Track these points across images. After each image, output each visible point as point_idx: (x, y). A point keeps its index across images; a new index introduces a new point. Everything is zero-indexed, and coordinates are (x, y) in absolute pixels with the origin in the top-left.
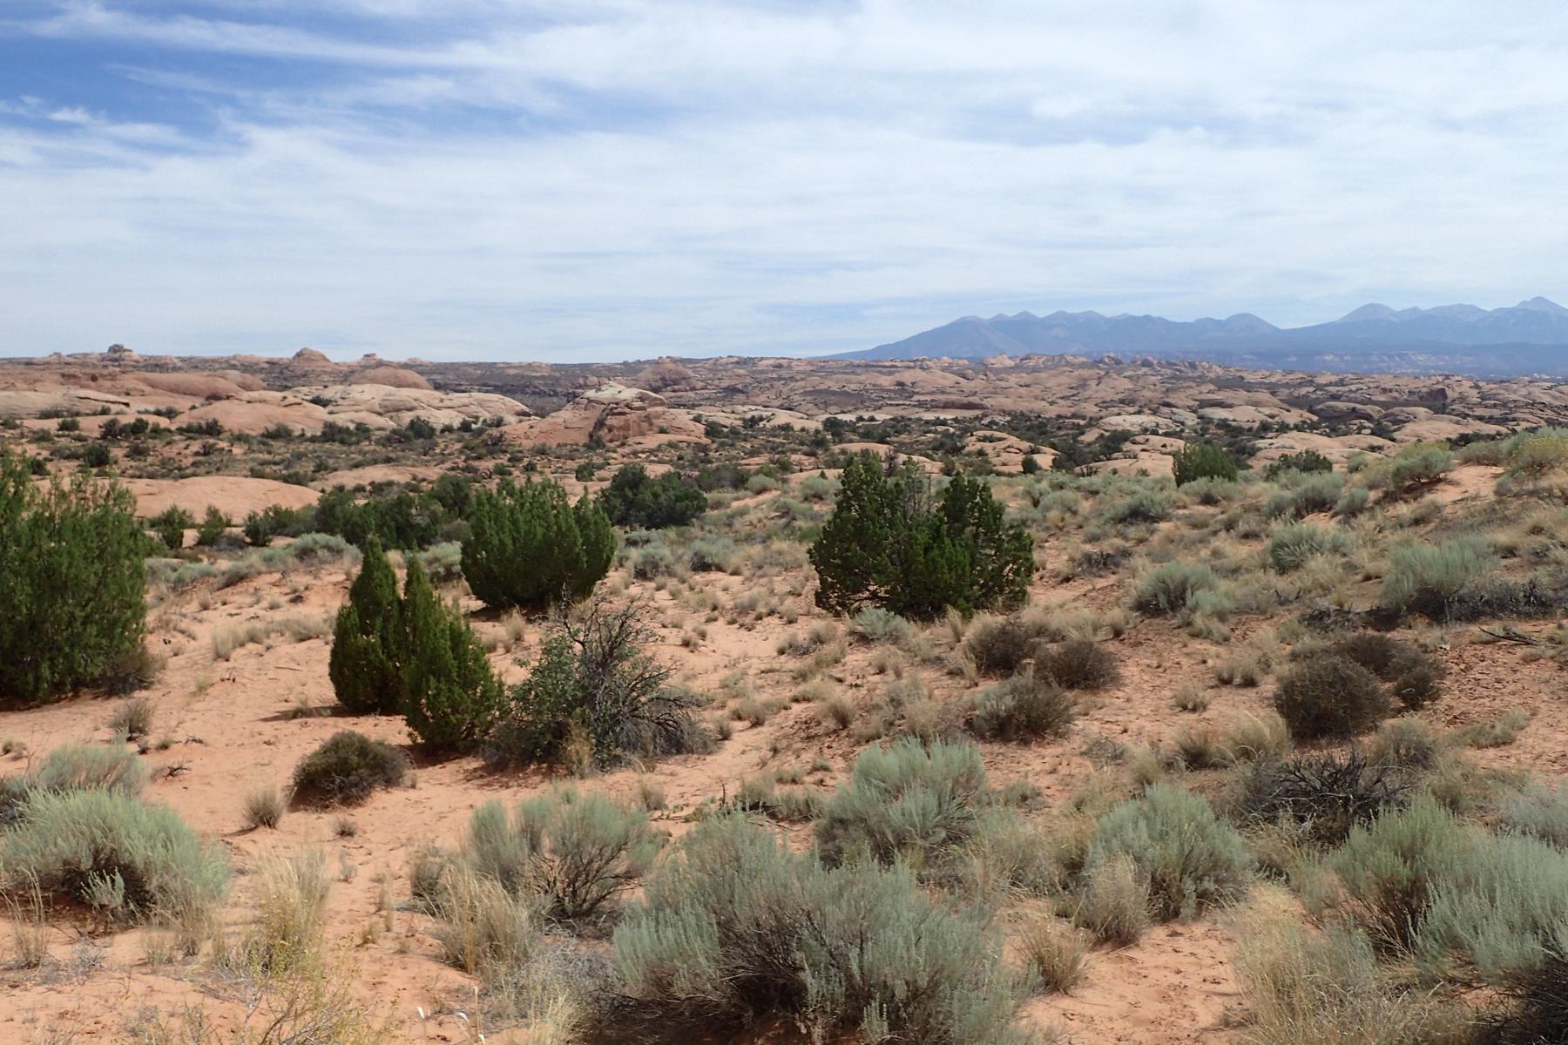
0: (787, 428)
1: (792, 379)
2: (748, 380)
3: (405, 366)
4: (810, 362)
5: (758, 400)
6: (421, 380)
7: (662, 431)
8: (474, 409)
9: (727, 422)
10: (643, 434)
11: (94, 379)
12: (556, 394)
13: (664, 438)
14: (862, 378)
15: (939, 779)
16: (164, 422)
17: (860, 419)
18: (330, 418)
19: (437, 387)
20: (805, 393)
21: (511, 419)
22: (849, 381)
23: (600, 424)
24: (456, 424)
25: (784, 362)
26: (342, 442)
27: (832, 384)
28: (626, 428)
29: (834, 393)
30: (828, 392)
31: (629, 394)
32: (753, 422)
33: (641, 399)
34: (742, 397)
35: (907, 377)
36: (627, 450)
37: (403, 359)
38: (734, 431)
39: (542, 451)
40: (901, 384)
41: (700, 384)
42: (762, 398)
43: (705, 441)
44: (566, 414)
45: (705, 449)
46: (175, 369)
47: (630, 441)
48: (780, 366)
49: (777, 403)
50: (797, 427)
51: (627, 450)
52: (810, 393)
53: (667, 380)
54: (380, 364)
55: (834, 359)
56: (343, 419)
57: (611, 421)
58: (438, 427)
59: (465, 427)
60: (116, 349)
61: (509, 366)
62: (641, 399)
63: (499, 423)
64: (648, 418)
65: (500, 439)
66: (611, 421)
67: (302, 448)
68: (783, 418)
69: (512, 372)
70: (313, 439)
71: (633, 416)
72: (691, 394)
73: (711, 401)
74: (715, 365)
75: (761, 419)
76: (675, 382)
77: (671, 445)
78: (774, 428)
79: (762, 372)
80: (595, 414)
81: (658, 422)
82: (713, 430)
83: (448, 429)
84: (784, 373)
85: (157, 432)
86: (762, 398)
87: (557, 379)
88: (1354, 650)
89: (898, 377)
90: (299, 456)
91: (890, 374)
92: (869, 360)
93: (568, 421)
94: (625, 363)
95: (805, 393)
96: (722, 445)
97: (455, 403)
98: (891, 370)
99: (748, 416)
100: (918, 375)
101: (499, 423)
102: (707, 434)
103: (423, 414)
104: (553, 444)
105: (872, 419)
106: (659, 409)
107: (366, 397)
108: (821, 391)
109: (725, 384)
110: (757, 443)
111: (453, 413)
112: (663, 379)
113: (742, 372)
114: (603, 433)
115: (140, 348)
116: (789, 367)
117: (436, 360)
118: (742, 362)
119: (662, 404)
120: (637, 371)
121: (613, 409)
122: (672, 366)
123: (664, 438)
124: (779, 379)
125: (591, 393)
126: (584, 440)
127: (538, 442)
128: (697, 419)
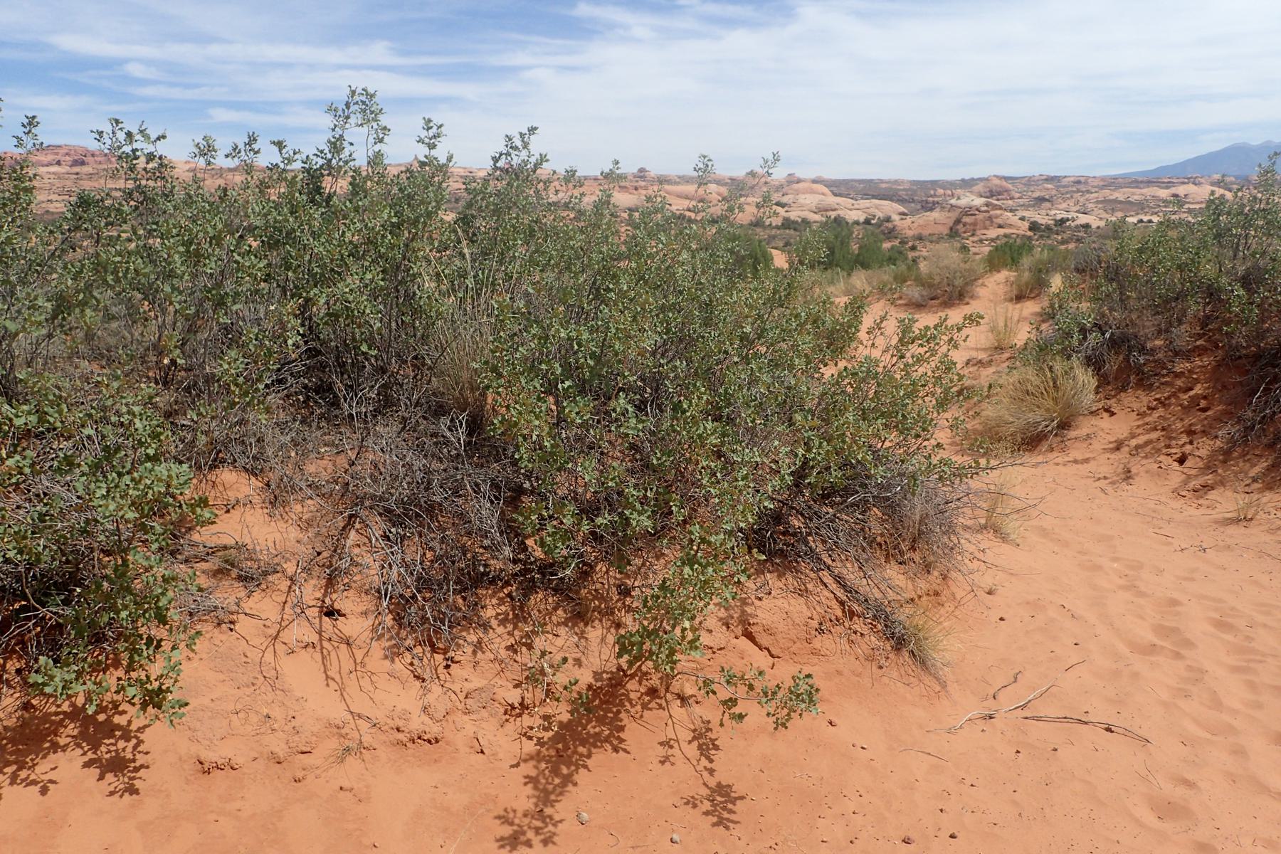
0: (1087, 226)
1: (1088, 192)
2: (1054, 192)
3: (814, 182)
4: (1103, 179)
5: (1061, 207)
6: (826, 190)
7: (1000, 226)
8: (872, 211)
9: (1043, 222)
10: (986, 228)
11: (636, 189)
12: (913, 201)
13: (1001, 231)
14: (1145, 191)
15: (594, 750)
16: (693, 215)
17: (1141, 221)
18: (787, 215)
19: (836, 195)
20: (1098, 202)
21: (895, 217)
22: (1134, 194)
23: (958, 221)
24: (862, 220)
25: (1083, 180)
26: (795, 230)
27: (1119, 195)
28: (975, 224)
29: (1121, 202)
30: (1116, 201)
31: (979, 202)
32: (1063, 221)
33: (987, 205)
34: (1048, 205)
35: (1181, 190)
36: (975, 239)
37: (813, 176)
38: (1048, 228)
39: (920, 238)
40: (1175, 196)
41: (1017, 195)
42: (1064, 205)
43: (1029, 233)
44: (936, 215)
45: (1030, 238)
46: (676, 183)
47: (978, 232)
48: (1079, 182)
49: (1076, 209)
50: (1094, 226)
51: (975, 239)
52: (1101, 202)
53: (995, 191)
54: (799, 181)
55: (1124, 177)
56: (794, 215)
57: (966, 219)
58: (850, 222)
59: (867, 222)
60: (642, 170)
61: (882, 181)
62: (987, 205)
63: (888, 219)
64: (990, 218)
65: (893, 229)
66: (966, 219)
67: (773, 232)
68: (1083, 219)
69: (884, 186)
70: (777, 227)
71: (980, 216)
72: (1010, 202)
73: (1026, 207)
74: (1029, 182)
75: (1068, 220)
76: (1000, 193)
77: (1005, 236)
78: (1077, 227)
79: (1064, 186)
80: (954, 215)
81: (999, 221)
82: (1034, 227)
83: (857, 223)
84: (1083, 188)
85: (690, 221)
86: (1064, 205)
87: (915, 191)
88: (1114, 274)
89: (1173, 190)
90: (774, 237)
91: (1167, 188)
92: (1150, 178)
93: (937, 219)
94: (963, 180)
95: (1098, 202)
96: (1041, 237)
97: (862, 206)
98: (1168, 185)
99: (1059, 217)
100: (1191, 188)
101: (888, 219)
102: (1030, 229)
103: (841, 213)
104: (926, 233)
105: (1150, 221)
106: (998, 212)
107: (808, 202)
108: (1110, 201)
109: (1037, 194)
110: (1065, 236)
111: (860, 213)
112: (991, 191)
113: (1050, 186)
114: (960, 227)
115: (655, 170)
116: (1086, 183)
117: (834, 178)
118: (1050, 179)
119: (1001, 208)
120: (971, 186)
121: (968, 211)
122: (997, 182)
123: (1001, 231)
124: (1078, 191)
125: (953, 201)
126: (946, 231)
127: (916, 232)
128: (1022, 219)
